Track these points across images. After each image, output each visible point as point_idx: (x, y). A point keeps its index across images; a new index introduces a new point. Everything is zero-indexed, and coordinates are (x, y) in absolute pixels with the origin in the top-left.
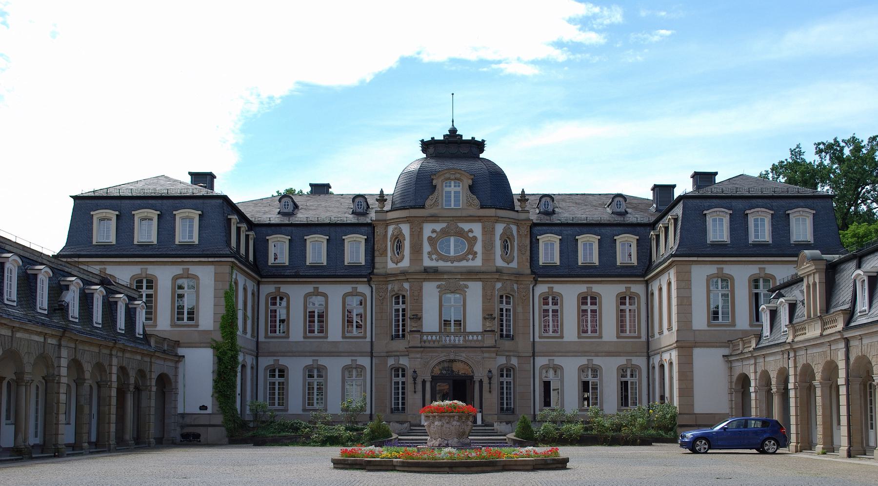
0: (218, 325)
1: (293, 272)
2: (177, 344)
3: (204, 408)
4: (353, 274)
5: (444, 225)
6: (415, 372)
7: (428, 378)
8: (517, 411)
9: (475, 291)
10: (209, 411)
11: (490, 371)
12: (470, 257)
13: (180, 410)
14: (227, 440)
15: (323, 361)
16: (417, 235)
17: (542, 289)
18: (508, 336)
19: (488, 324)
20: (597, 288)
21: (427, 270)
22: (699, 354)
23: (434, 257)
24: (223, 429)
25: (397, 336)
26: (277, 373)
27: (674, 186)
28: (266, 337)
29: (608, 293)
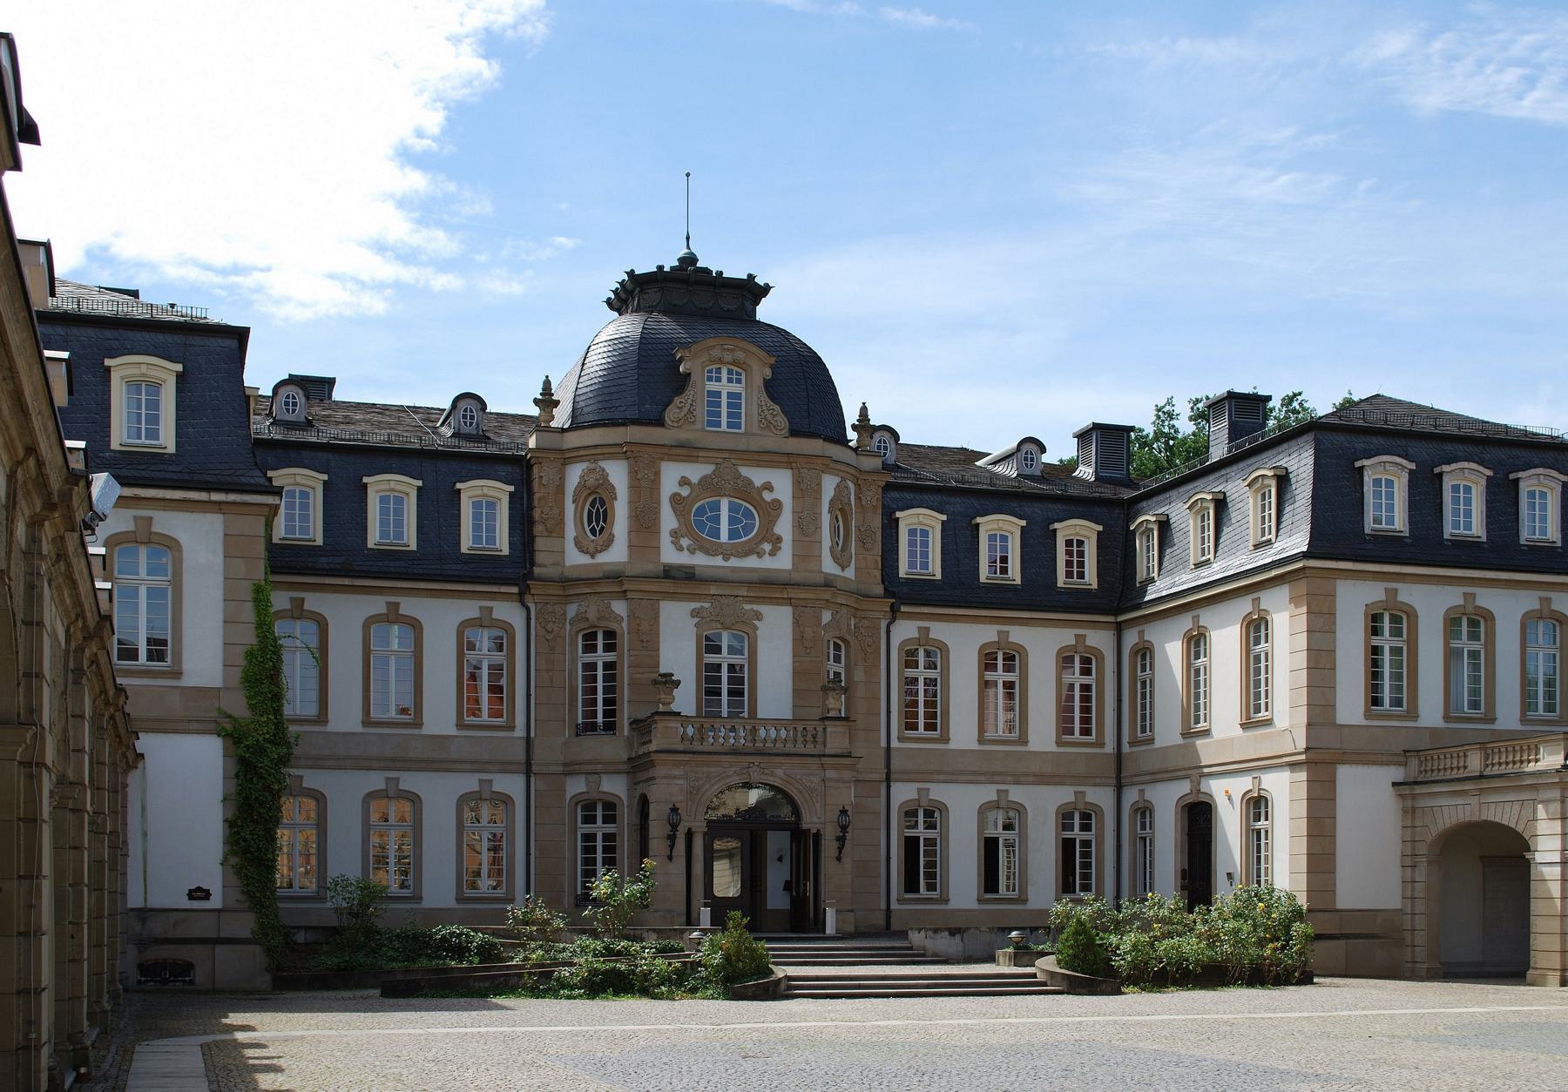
0: (237, 674)
4: (481, 573)
5: (708, 469)
6: (674, 810)
7: (700, 826)
10: (216, 902)
12: (767, 547)
13: (135, 900)
14: (268, 977)
17: (905, 630)
20: (1019, 635)
22: (1346, 775)
24: (258, 949)
25: (590, 727)
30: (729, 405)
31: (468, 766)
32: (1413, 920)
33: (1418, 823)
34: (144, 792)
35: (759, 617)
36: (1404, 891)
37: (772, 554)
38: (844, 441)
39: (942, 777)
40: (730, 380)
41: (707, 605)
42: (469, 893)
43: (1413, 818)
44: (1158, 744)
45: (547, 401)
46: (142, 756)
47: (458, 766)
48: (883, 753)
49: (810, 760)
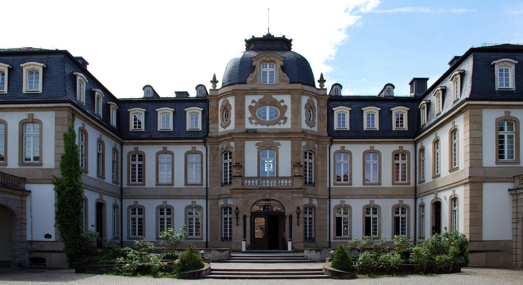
0: (59, 164)
1: (147, 136)
2: (25, 180)
3: (48, 236)
4: (193, 137)
5: (261, 97)
6: (237, 208)
7: (248, 214)
8: (317, 240)
9: (285, 148)
10: (53, 239)
11: (298, 208)
12: (282, 121)
13: (29, 238)
14: (68, 264)
15: (170, 202)
16: (240, 105)
17: (336, 148)
18: (310, 183)
19: (296, 170)
21: (248, 132)
22: (487, 188)
23: (254, 121)
24: (64, 255)
25: (226, 183)
26: (137, 211)
27: (427, 79)
28: (129, 184)
29: (387, 150)
30: (270, 75)
31: (188, 197)
32: (516, 244)
33: (519, 205)
34: (31, 203)
36: (513, 232)
37: (284, 123)
38: (313, 85)
39: (349, 197)
40: (270, 67)
41: (261, 142)
43: (517, 203)
44: (426, 182)
45: (214, 81)
46: (30, 191)
47: (185, 197)
48: (327, 189)
49: (287, 191)
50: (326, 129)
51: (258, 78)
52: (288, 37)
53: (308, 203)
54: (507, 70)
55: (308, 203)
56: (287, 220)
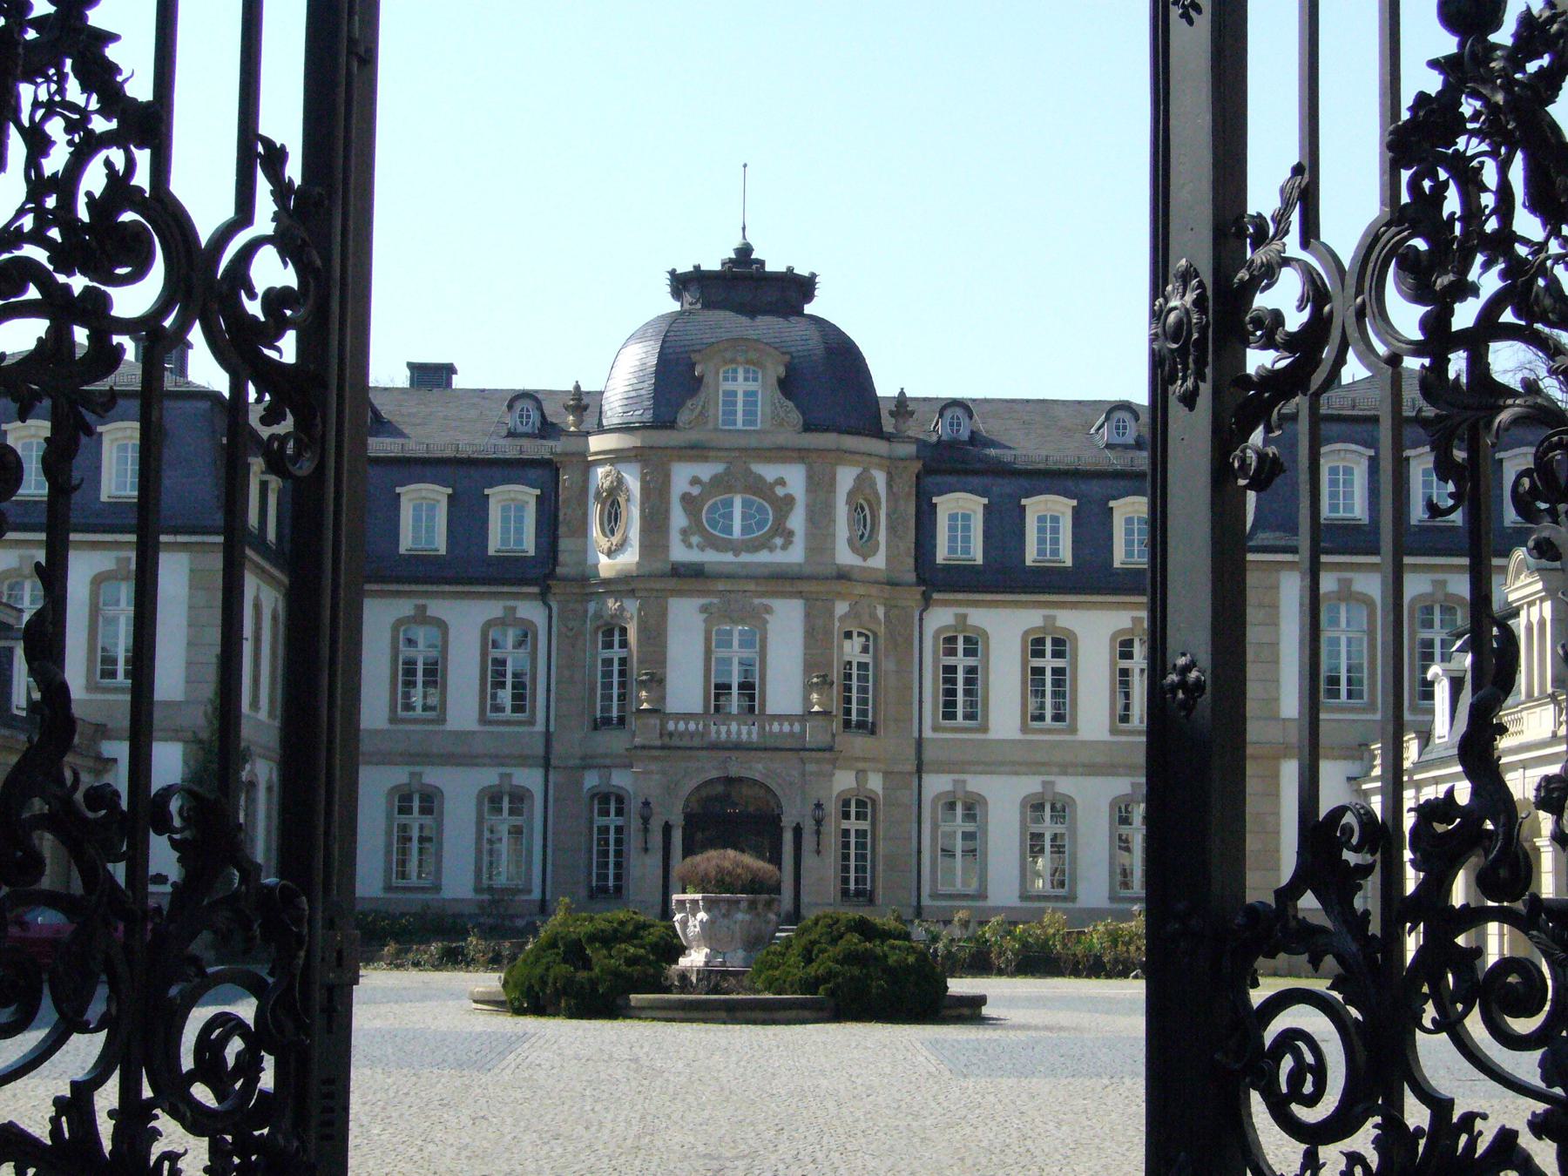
4: (507, 574)
5: (719, 468)
6: (646, 804)
7: (677, 819)
11: (819, 806)
12: (779, 541)
17: (940, 618)
25: (607, 721)
30: (745, 404)
35: (768, 610)
37: (784, 547)
40: (746, 379)
41: (716, 601)
42: (395, 882)
48: (913, 743)
50: (911, 561)
51: (711, 412)
52: (802, 270)
53: (854, 785)
54: (1348, 471)
55: (854, 785)
56: (788, 837)
